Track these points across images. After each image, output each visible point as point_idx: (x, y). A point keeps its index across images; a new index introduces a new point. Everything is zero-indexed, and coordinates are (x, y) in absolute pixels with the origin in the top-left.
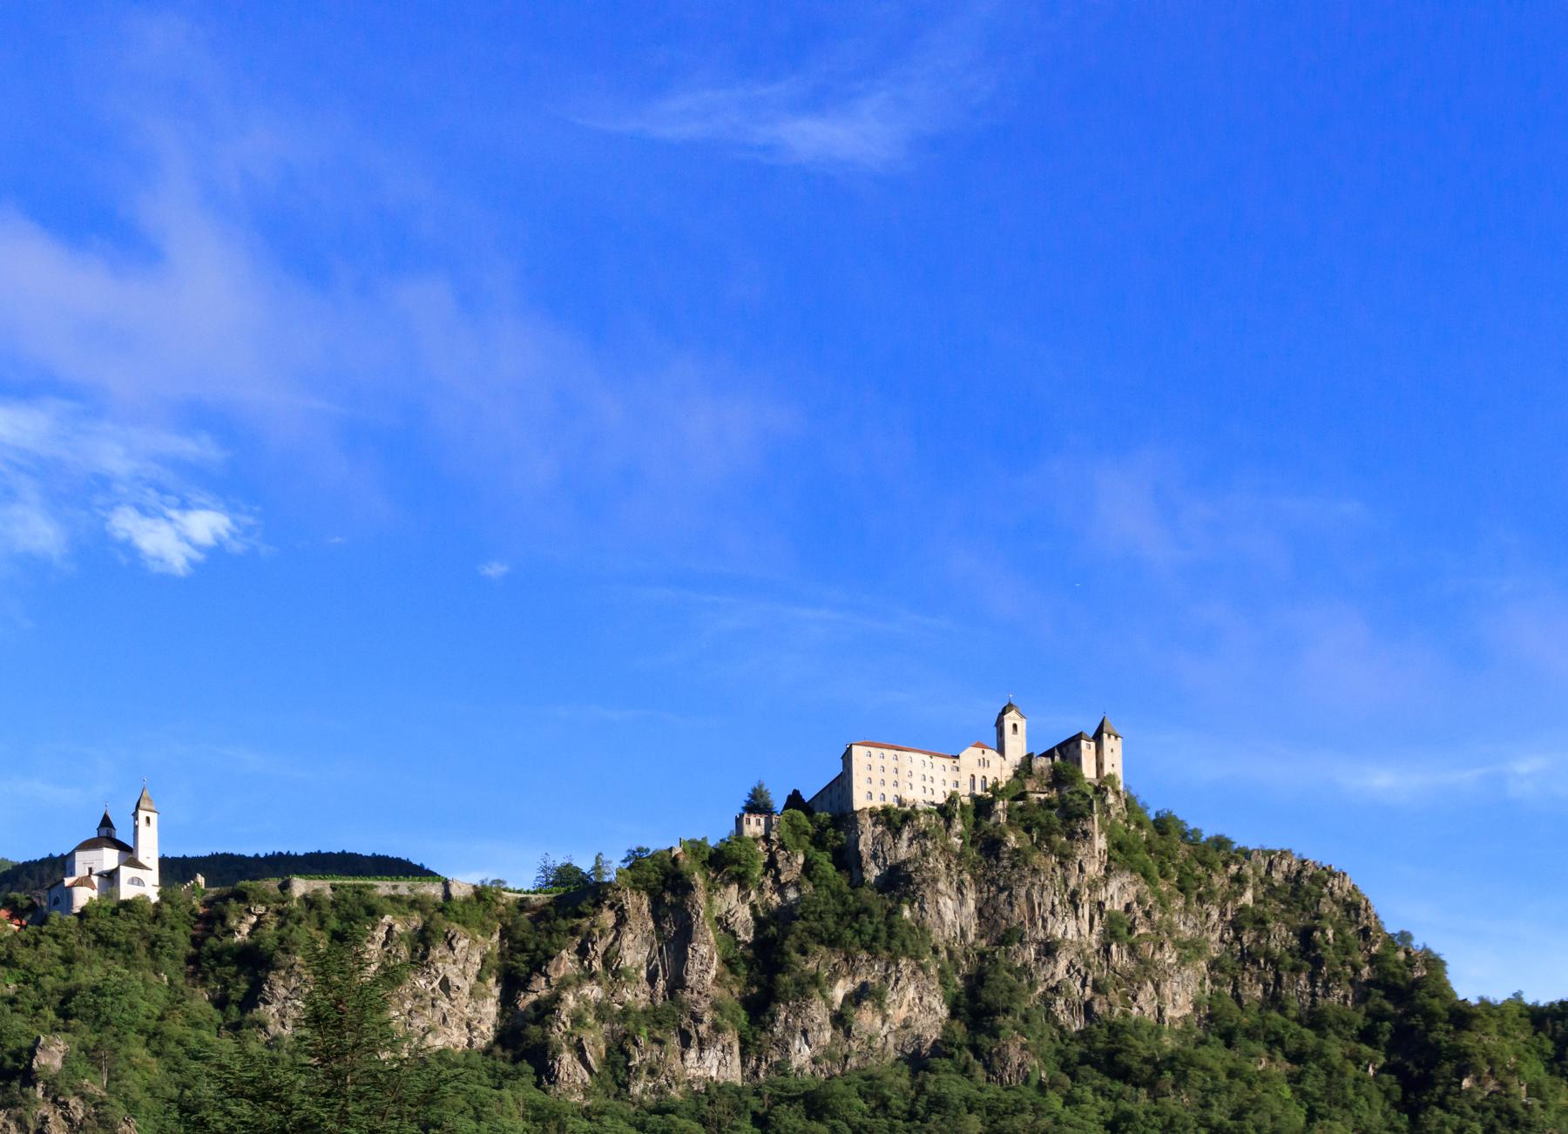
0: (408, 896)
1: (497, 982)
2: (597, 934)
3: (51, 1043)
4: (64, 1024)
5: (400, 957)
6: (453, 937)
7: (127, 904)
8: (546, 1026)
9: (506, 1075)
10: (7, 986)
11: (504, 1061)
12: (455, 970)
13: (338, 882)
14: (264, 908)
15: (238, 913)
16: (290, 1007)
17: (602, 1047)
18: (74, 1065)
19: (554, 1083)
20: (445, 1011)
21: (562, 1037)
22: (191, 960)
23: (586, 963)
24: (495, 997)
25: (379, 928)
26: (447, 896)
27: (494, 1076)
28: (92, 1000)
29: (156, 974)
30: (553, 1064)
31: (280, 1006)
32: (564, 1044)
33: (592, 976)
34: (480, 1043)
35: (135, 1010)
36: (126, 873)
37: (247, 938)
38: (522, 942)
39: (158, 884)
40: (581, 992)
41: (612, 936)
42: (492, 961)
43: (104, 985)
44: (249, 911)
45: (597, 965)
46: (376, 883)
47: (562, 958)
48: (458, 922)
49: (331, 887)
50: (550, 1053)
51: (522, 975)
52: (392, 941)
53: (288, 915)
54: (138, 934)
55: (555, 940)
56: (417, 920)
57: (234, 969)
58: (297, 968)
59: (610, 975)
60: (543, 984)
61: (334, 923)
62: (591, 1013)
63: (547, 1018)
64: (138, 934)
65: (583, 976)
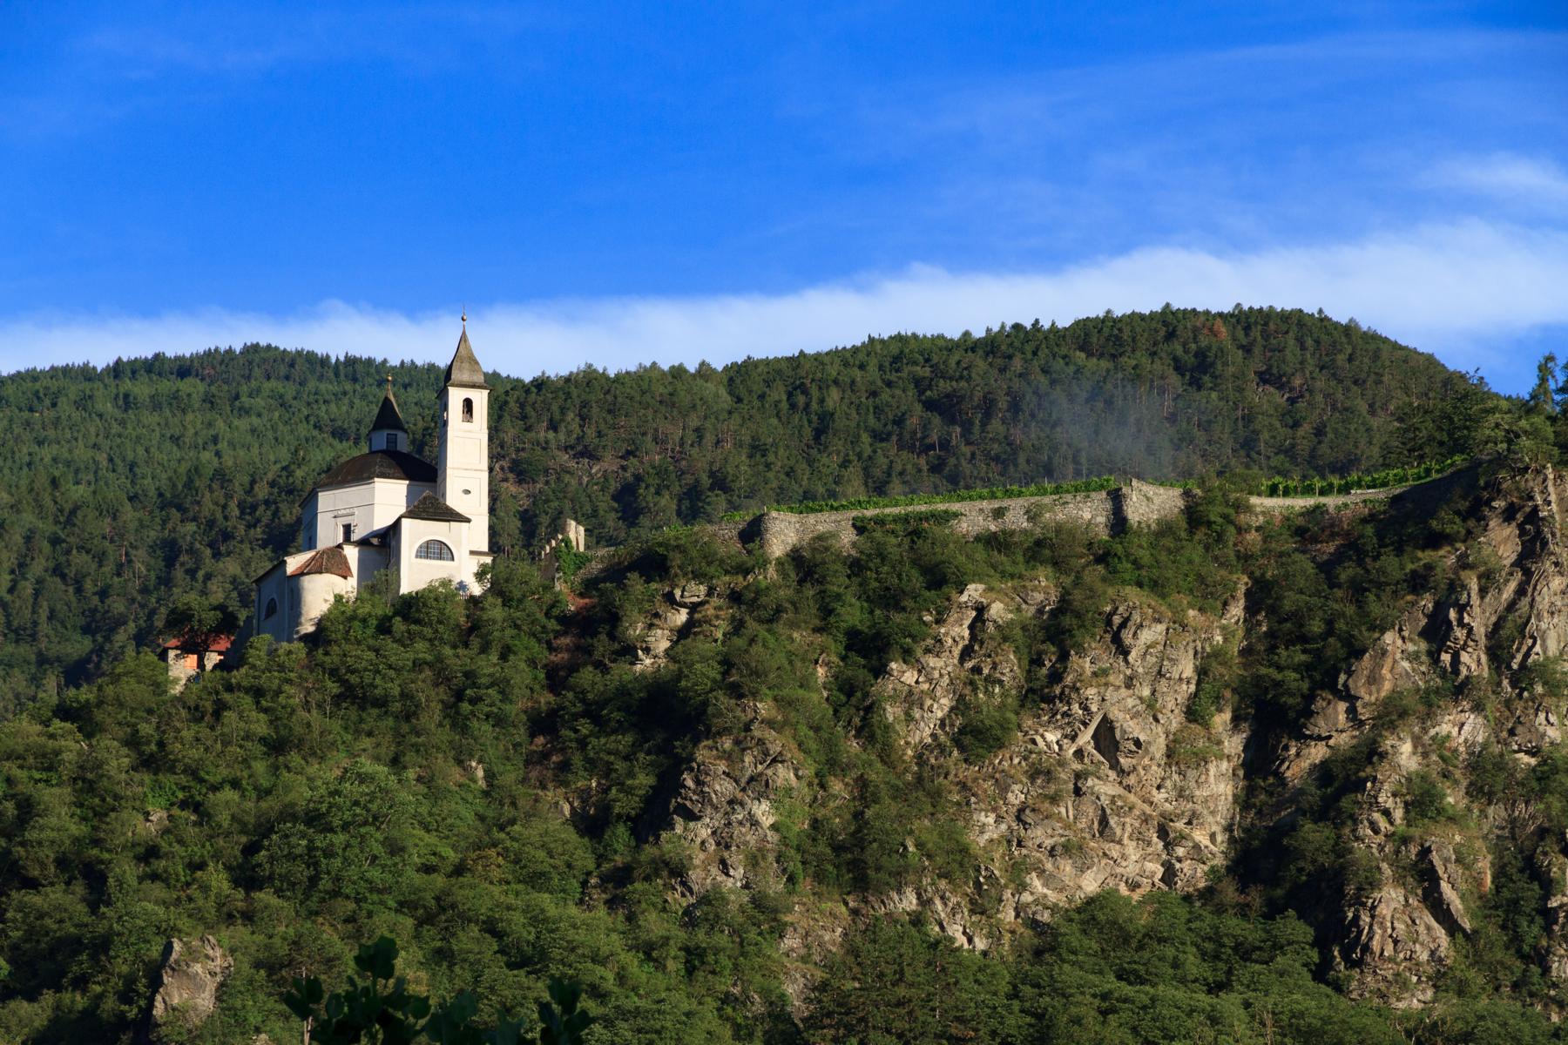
0: (1024, 532)
1: (1236, 720)
2: (1474, 586)
3: (192, 955)
4: (245, 900)
5: (1001, 682)
6: (1123, 625)
7: (411, 607)
8: (1343, 823)
9: (1245, 952)
10: (147, 814)
11: (1244, 916)
12: (1130, 702)
13: (870, 513)
14: (703, 589)
15: (647, 606)
16: (741, 823)
17: (1485, 866)
18: (238, 1004)
19: (1359, 964)
20: (1105, 801)
21: (1381, 848)
22: (543, 723)
23: (1446, 658)
24: (1229, 757)
25: (954, 616)
26: (1119, 523)
27: (1217, 957)
28: (304, 842)
29: (460, 762)
30: (1356, 918)
31: (718, 821)
32: (1384, 866)
33: (1459, 689)
34: (1193, 874)
35: (397, 859)
36: (415, 533)
37: (662, 662)
38: (1297, 617)
39: (485, 549)
40: (1432, 732)
41: (1512, 586)
42: (1223, 670)
43: (331, 806)
44: (670, 599)
45: (1474, 662)
46: (955, 507)
47: (1384, 653)
48: (1140, 585)
49: (854, 525)
50: (1350, 890)
51: (1291, 701)
52: (982, 643)
53: (755, 600)
54: (428, 672)
55: (1375, 608)
56: (1044, 588)
57: (625, 740)
58: (757, 731)
59: (1505, 682)
60: (1342, 717)
61: (853, 613)
62: (1456, 782)
63: (1345, 802)
64: (428, 672)
65: (1437, 691)
